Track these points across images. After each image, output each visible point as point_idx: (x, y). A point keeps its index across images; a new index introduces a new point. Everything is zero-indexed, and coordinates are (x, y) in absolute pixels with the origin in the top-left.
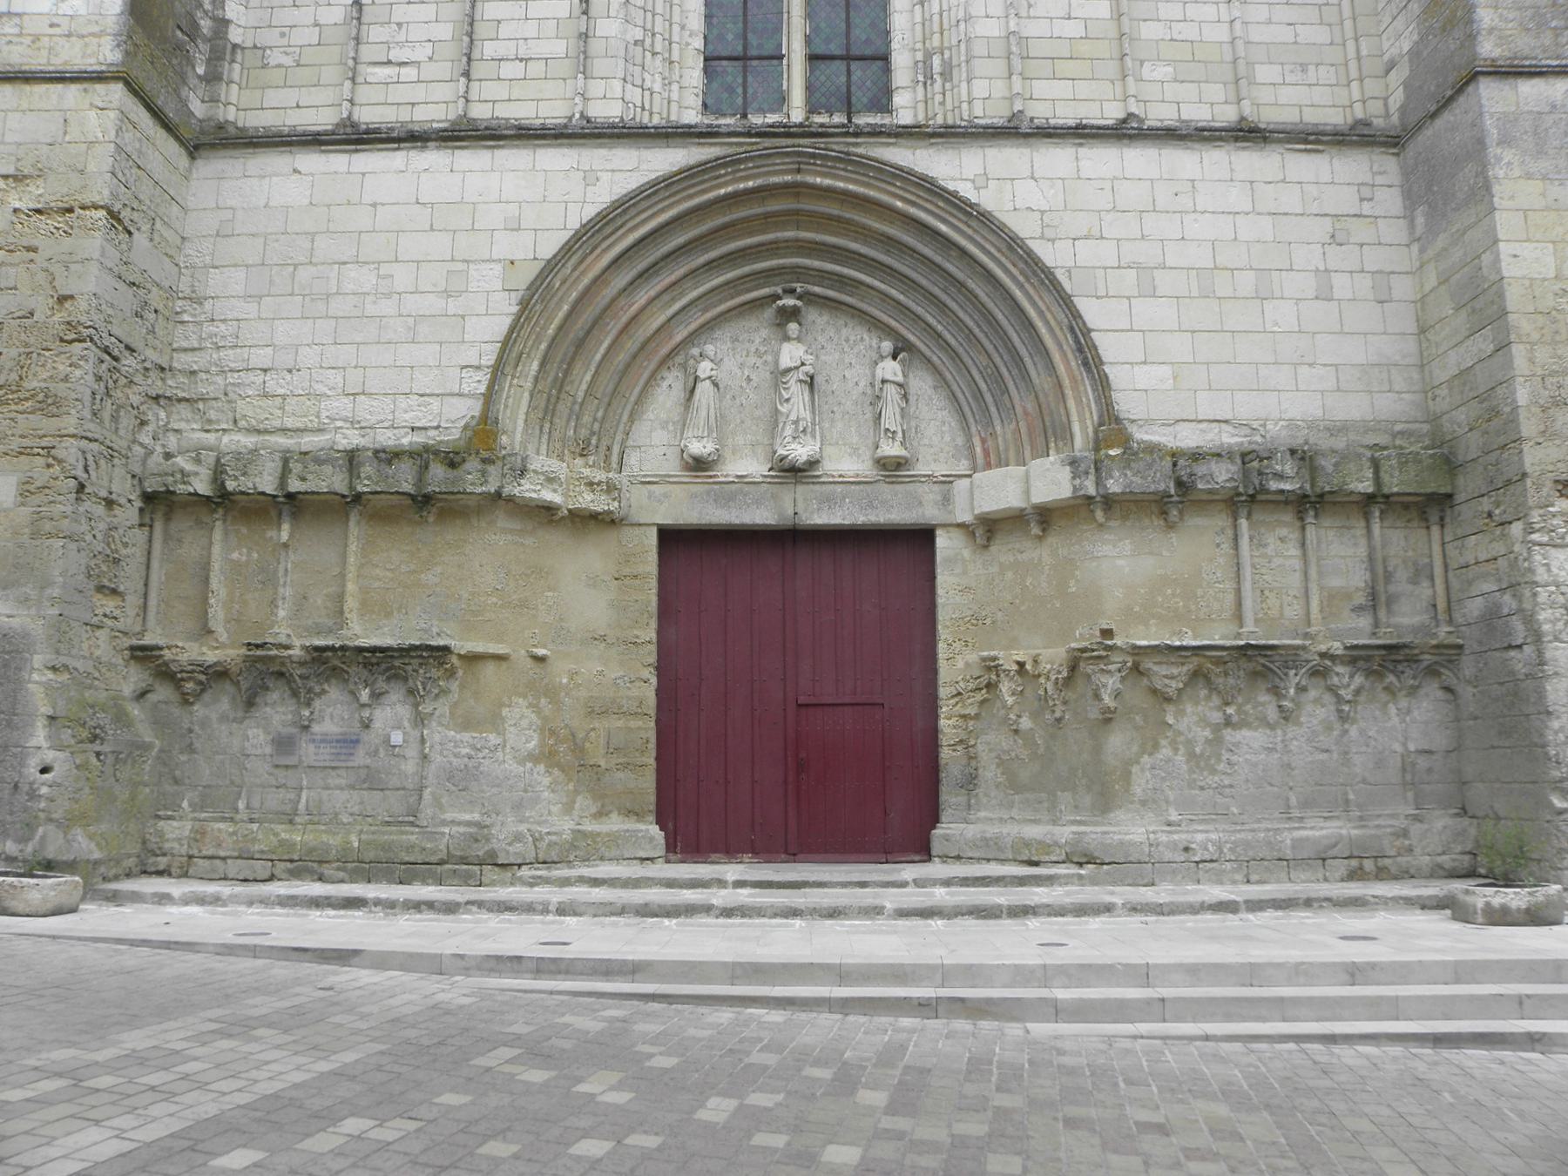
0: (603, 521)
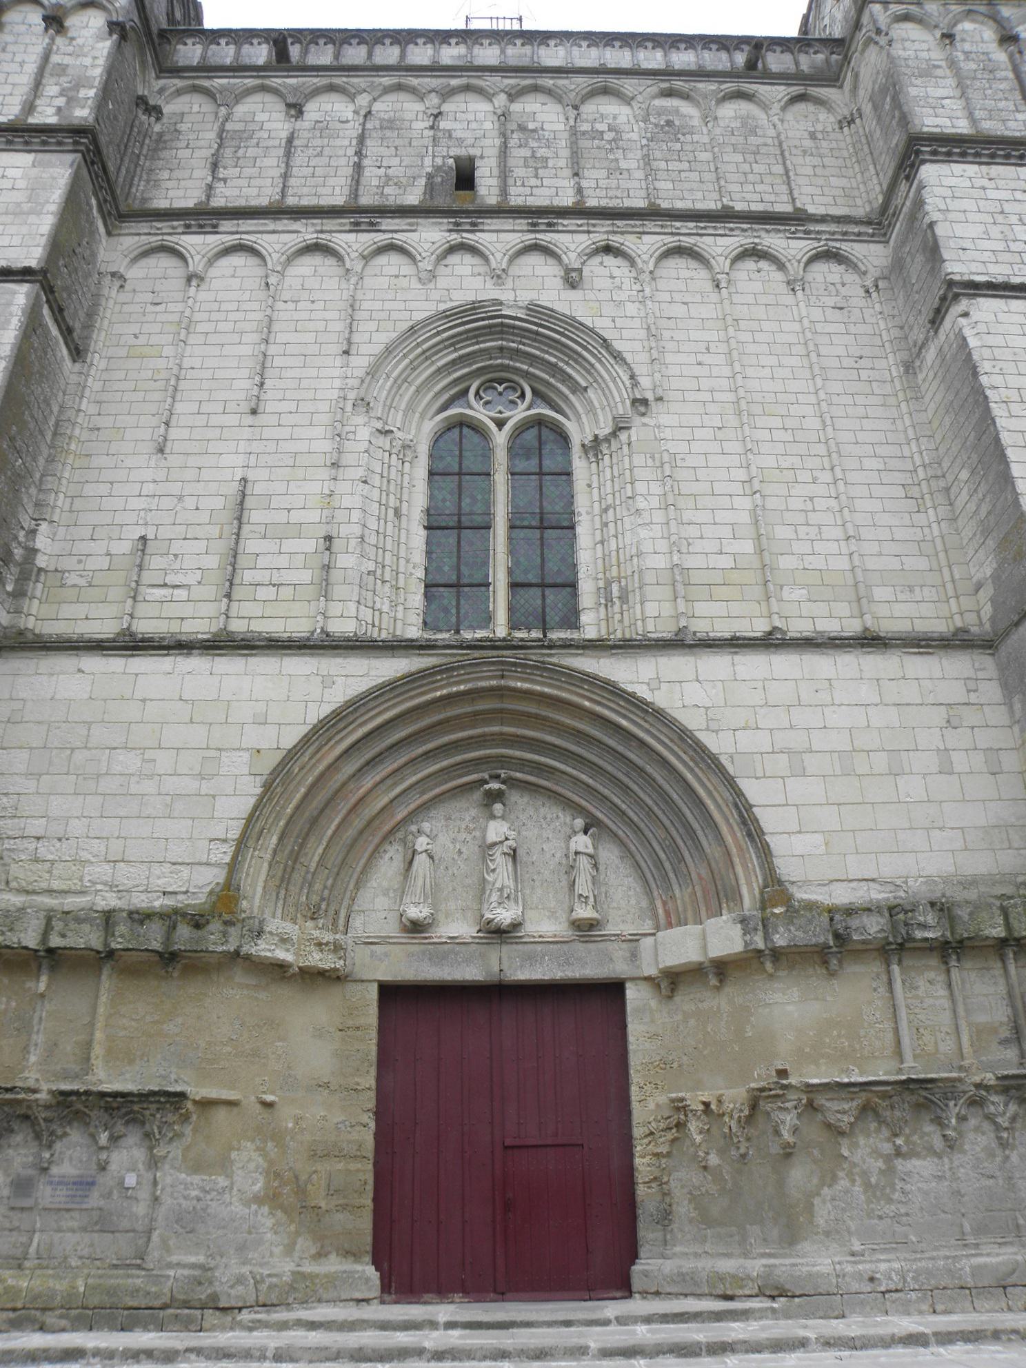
0: (330, 977)
